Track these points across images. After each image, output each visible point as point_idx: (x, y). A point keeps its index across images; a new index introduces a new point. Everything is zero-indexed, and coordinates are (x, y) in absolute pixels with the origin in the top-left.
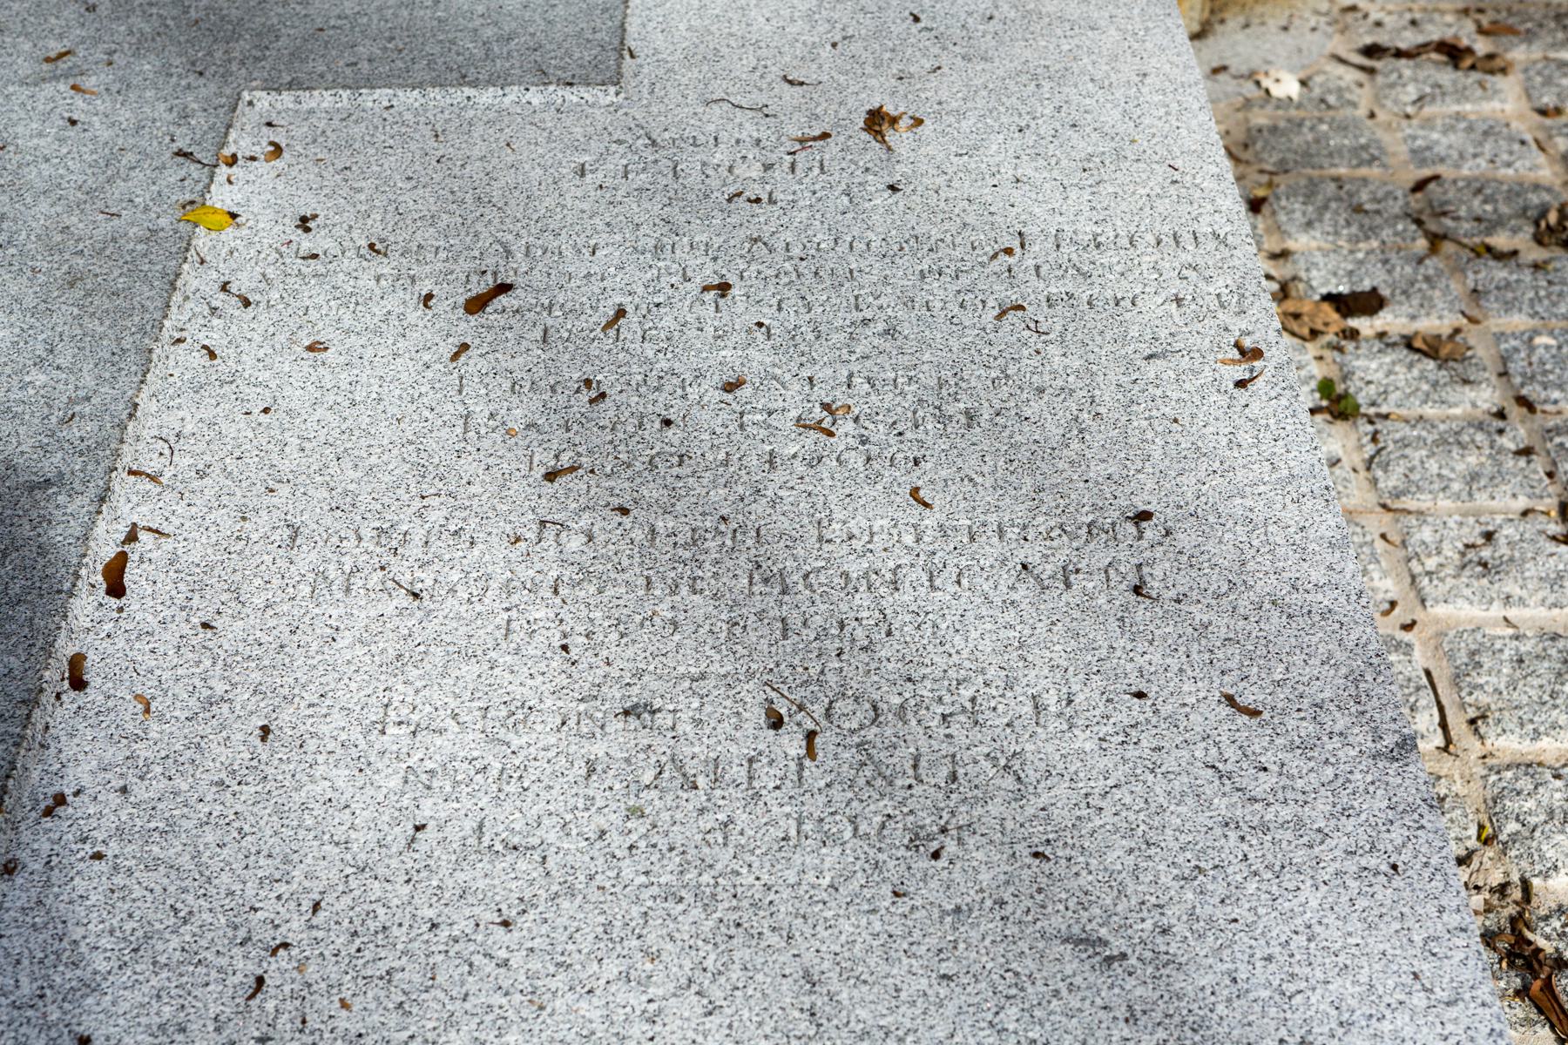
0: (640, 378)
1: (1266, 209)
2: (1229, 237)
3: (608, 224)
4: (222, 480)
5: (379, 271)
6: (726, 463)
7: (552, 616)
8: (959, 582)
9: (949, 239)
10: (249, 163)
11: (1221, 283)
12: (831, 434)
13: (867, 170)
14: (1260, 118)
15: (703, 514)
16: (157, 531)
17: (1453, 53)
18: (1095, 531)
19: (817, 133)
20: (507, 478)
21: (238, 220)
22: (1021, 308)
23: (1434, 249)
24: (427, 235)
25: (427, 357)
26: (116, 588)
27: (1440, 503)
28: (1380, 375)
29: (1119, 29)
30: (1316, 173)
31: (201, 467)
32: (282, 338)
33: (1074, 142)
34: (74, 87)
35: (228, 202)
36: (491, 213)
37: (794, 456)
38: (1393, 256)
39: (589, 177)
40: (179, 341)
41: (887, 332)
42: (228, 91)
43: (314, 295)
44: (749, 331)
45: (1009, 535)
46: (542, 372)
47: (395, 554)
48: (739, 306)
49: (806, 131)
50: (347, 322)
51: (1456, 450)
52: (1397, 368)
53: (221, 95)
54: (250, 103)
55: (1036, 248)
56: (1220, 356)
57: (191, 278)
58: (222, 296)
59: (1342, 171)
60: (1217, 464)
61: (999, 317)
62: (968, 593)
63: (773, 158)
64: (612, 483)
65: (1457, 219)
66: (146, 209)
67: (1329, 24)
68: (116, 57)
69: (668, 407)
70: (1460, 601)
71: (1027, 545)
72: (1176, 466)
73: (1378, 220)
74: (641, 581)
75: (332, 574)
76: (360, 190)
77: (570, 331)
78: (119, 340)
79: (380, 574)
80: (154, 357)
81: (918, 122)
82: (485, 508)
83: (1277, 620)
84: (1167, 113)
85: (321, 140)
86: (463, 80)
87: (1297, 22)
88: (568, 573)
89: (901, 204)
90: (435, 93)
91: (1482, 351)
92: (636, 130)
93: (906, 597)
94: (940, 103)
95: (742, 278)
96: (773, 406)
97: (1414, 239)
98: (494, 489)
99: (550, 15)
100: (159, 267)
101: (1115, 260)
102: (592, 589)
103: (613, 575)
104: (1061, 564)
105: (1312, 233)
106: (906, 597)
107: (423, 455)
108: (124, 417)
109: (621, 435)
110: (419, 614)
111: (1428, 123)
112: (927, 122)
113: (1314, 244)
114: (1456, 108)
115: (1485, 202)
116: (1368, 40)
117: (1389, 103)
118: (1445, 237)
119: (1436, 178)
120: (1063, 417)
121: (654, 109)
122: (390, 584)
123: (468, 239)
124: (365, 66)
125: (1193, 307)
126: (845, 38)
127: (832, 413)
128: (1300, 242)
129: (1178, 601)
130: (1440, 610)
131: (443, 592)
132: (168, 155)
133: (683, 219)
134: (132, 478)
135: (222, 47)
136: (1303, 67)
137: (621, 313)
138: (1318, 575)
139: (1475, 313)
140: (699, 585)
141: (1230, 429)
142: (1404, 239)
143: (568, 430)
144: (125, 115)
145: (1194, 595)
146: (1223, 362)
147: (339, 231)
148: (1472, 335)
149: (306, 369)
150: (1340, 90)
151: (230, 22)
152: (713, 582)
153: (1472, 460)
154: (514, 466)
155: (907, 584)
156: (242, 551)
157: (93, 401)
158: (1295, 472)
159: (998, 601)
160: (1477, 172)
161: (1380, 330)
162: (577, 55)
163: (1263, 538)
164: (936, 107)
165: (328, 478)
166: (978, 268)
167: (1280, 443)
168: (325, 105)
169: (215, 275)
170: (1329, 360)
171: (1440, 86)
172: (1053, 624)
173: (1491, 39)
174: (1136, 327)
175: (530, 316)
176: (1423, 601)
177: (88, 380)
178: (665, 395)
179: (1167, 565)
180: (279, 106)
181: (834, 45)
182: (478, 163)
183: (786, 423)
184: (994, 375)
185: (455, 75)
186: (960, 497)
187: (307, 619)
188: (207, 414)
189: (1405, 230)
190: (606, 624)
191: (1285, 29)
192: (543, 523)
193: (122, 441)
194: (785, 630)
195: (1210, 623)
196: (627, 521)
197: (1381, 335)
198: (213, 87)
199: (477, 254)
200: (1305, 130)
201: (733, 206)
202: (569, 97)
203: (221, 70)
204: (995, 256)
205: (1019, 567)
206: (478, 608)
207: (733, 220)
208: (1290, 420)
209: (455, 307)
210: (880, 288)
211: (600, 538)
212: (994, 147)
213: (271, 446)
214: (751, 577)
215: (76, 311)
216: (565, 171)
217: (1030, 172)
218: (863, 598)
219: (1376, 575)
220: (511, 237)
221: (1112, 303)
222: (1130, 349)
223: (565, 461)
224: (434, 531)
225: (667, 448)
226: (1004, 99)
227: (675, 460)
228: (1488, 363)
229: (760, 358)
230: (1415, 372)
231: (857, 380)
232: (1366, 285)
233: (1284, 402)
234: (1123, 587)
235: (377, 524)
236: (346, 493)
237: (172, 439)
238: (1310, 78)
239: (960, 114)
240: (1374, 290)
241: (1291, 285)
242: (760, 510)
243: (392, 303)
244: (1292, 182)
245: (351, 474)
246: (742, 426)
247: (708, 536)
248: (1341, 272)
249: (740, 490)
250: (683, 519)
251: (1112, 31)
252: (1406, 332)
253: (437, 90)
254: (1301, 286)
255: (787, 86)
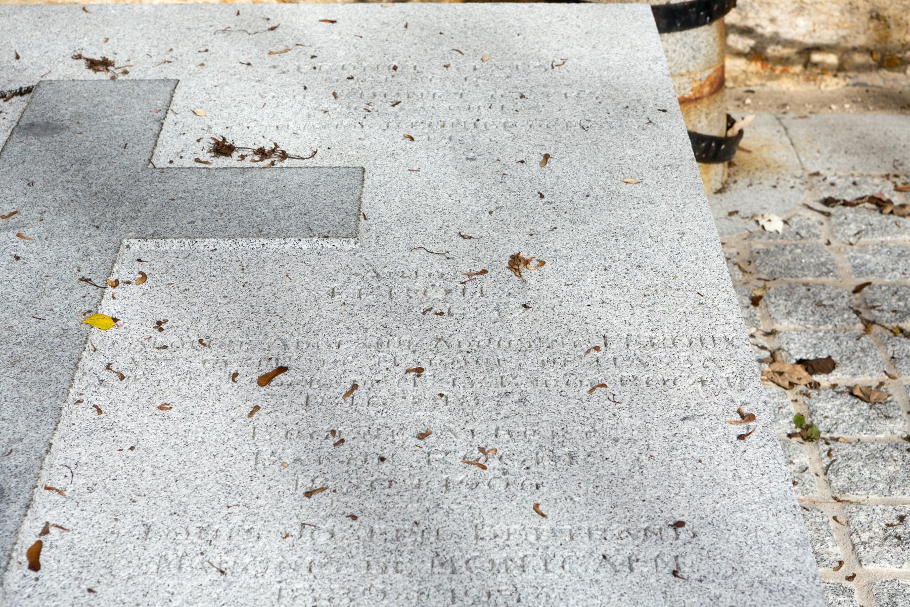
0: (366, 429)
1: (761, 303)
2: (735, 340)
3: (348, 328)
4: (103, 493)
5: (205, 357)
6: (418, 486)
7: (307, 586)
8: (563, 567)
9: (560, 340)
10: (126, 286)
11: (729, 371)
12: (484, 468)
13: (510, 294)
14: (758, 245)
15: (404, 520)
16: (61, 528)
17: (880, 203)
18: (649, 534)
19: (479, 270)
20: (281, 494)
21: (118, 322)
22: (604, 385)
23: (867, 330)
24: (236, 334)
25: (233, 414)
26: (35, 566)
27: (870, 497)
28: (833, 412)
29: (667, 203)
30: (793, 280)
31: (90, 485)
32: (143, 401)
33: (639, 277)
34: (18, 235)
35: (112, 310)
36: (275, 320)
37: (461, 482)
38: (841, 334)
39: (337, 297)
40: (79, 402)
41: (521, 401)
42: (114, 239)
43: (164, 372)
44: (434, 399)
45: (595, 536)
46: (305, 425)
47: (210, 544)
48: (429, 386)
49: (473, 268)
50: (184, 391)
51: (880, 461)
52: (844, 408)
53: (109, 241)
54: (128, 246)
55: (614, 346)
56: (728, 419)
57: (88, 361)
58: (107, 372)
59: (810, 279)
60: (726, 490)
61: (591, 391)
62: (569, 575)
63: (451, 286)
64: (346, 499)
65: (882, 311)
66: (61, 315)
67: (802, 184)
68: (45, 215)
69: (383, 449)
70: (883, 562)
71: (606, 543)
72: (700, 491)
73: (832, 311)
74: (364, 564)
75: (170, 557)
76: (194, 304)
77: (323, 398)
78: (41, 401)
79: (200, 557)
80: (63, 413)
81: (542, 263)
82: (267, 515)
83: (762, 593)
84: (696, 259)
85: (171, 270)
86: (260, 234)
87: (782, 183)
88: (319, 558)
89: (530, 317)
90: (242, 241)
91: (897, 396)
92: (366, 267)
93: (530, 577)
94: (556, 251)
95: (431, 364)
96: (448, 449)
97: (854, 324)
98: (273, 502)
99: (315, 192)
100: (68, 354)
101: (663, 355)
102: (333, 570)
103: (346, 560)
104: (628, 555)
105: (791, 319)
106: (530, 577)
107: (229, 479)
108: (43, 452)
109: (353, 467)
110: (224, 584)
111: (863, 249)
112: (548, 263)
113: (792, 326)
114: (881, 239)
115: (899, 300)
116: (826, 195)
117: (839, 235)
118: (874, 322)
119: (869, 284)
120: (630, 458)
121: (378, 253)
122: (206, 564)
123: (261, 337)
124: (199, 224)
125: (712, 386)
126: (497, 208)
127: (485, 454)
128: (783, 325)
129: (701, 581)
130: (871, 567)
131: (239, 570)
132: (76, 280)
133: (395, 325)
134: (47, 491)
135: (112, 209)
136: (785, 212)
137: (355, 387)
138: (788, 564)
139: (892, 372)
140: (400, 567)
141: (734, 467)
142: (848, 324)
143: (320, 463)
144: (50, 254)
145: (711, 577)
146: (730, 423)
147: (181, 331)
148: (891, 387)
149: (158, 421)
150: (808, 226)
151: (116, 194)
152: (409, 565)
153: (891, 468)
154: (286, 487)
155: (531, 568)
156: (115, 541)
157: (24, 441)
158: (775, 496)
159: (587, 580)
160: (894, 280)
161: (833, 383)
162: (331, 218)
163: (754, 539)
164: (553, 253)
165: (169, 494)
166: (578, 359)
167: (766, 476)
168: (174, 248)
169: (102, 358)
170: (801, 402)
171: (871, 225)
172: (622, 595)
173: (903, 194)
174: (676, 399)
175: (298, 388)
176: (860, 561)
177: (22, 428)
178: (381, 441)
179: (694, 557)
180: (145, 248)
181: (491, 213)
182: (269, 287)
183: (456, 460)
184: (586, 430)
185: (255, 230)
186: (564, 510)
187: (154, 587)
188: (95, 449)
189: (849, 318)
190: (341, 592)
191: (775, 187)
192: (303, 525)
193: (41, 468)
194: (453, 598)
195: (721, 596)
196: (356, 524)
197: (834, 386)
198: (105, 236)
199: (266, 346)
200: (787, 252)
201: (426, 317)
202: (325, 245)
203: (111, 225)
204: (588, 352)
205: (601, 557)
206: (261, 581)
207: (426, 326)
208: (771, 462)
209: (251, 382)
210: (516, 371)
211: (339, 535)
212: (589, 280)
213: (134, 472)
214: (433, 562)
215: (15, 382)
216: (322, 293)
217: (611, 297)
218: (502, 577)
219: (830, 544)
220: (287, 336)
221: (661, 383)
222: (672, 414)
223: (318, 484)
224: (235, 530)
225: (382, 476)
226: (596, 249)
227: (387, 484)
228: (901, 405)
229: (440, 417)
230: (855, 411)
231: (501, 432)
232: (824, 355)
233: (768, 449)
234: (666, 571)
235: (199, 525)
236: (180, 503)
237: (73, 467)
238: (789, 219)
239: (569, 258)
240: (829, 357)
241: (777, 353)
242: (439, 518)
243: (212, 379)
244: (778, 286)
245: (184, 491)
246: (429, 462)
247: (407, 534)
248: (809, 345)
249: (427, 504)
250: (391, 523)
251: (664, 206)
252: (849, 384)
253: (244, 240)
254: (783, 354)
255: (461, 239)
